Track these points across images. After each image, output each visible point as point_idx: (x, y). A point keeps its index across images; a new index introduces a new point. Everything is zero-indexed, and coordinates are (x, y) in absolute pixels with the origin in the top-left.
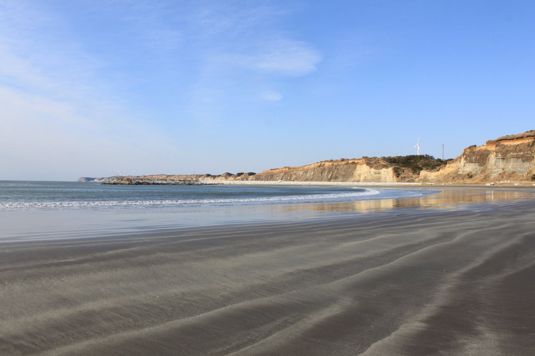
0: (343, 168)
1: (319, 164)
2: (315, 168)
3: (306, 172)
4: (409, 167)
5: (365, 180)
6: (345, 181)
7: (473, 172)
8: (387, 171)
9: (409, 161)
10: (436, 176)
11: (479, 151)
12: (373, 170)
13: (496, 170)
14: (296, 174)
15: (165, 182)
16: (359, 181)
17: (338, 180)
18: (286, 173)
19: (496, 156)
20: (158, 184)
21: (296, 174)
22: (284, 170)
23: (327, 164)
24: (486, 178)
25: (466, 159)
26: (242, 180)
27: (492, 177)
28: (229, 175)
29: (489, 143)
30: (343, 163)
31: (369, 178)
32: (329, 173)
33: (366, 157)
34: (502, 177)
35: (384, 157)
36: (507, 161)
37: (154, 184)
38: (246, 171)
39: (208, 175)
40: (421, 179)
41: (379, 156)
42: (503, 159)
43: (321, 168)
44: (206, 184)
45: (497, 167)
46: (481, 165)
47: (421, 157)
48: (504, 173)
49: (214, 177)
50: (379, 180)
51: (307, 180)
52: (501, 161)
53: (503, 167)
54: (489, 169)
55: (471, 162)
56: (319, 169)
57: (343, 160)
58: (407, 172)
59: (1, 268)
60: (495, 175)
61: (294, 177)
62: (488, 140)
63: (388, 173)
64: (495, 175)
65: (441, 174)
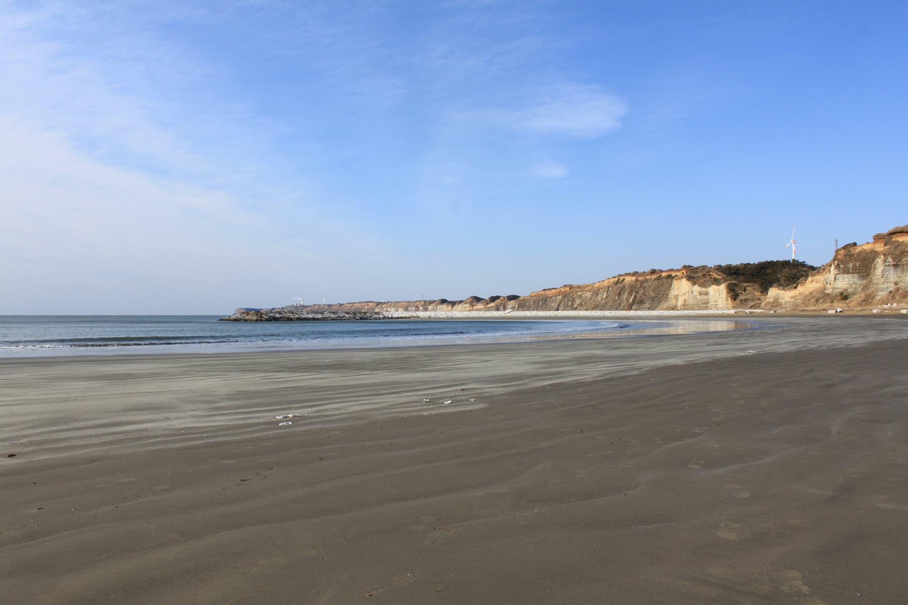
0: (649, 288)
1: (616, 279)
2: (609, 287)
3: (596, 293)
4: (755, 282)
5: (685, 306)
6: (653, 309)
7: (850, 290)
8: (719, 290)
9: (763, 272)
10: (792, 297)
11: (860, 253)
12: (697, 288)
13: (884, 286)
14: (580, 296)
15: (319, 316)
16: (674, 308)
17: (644, 306)
18: (565, 295)
19: (885, 261)
20: (306, 319)
21: (580, 296)
22: (563, 290)
23: (628, 279)
24: (868, 300)
25: (838, 267)
26: (497, 309)
27: (878, 298)
28: (477, 300)
29: (878, 238)
30: (654, 277)
31: (691, 301)
32: (630, 294)
33: (689, 266)
34: (893, 298)
35: (720, 266)
36: (903, 270)
37: (299, 319)
38: (505, 293)
39: (444, 301)
40: (769, 303)
41: (711, 264)
42: (896, 266)
43: (619, 285)
44: (392, 318)
45: (886, 281)
46: (862, 277)
47: (785, 264)
48: (898, 290)
49: (453, 304)
50: (705, 305)
51: (595, 308)
52: (892, 269)
53: (896, 279)
54: (874, 284)
55: (846, 271)
56: (616, 288)
57: (653, 272)
58: (751, 290)
59: (2, 436)
60: (884, 293)
61: (578, 302)
62: (875, 234)
63: (718, 294)
64: (884, 293)
65: (800, 294)
